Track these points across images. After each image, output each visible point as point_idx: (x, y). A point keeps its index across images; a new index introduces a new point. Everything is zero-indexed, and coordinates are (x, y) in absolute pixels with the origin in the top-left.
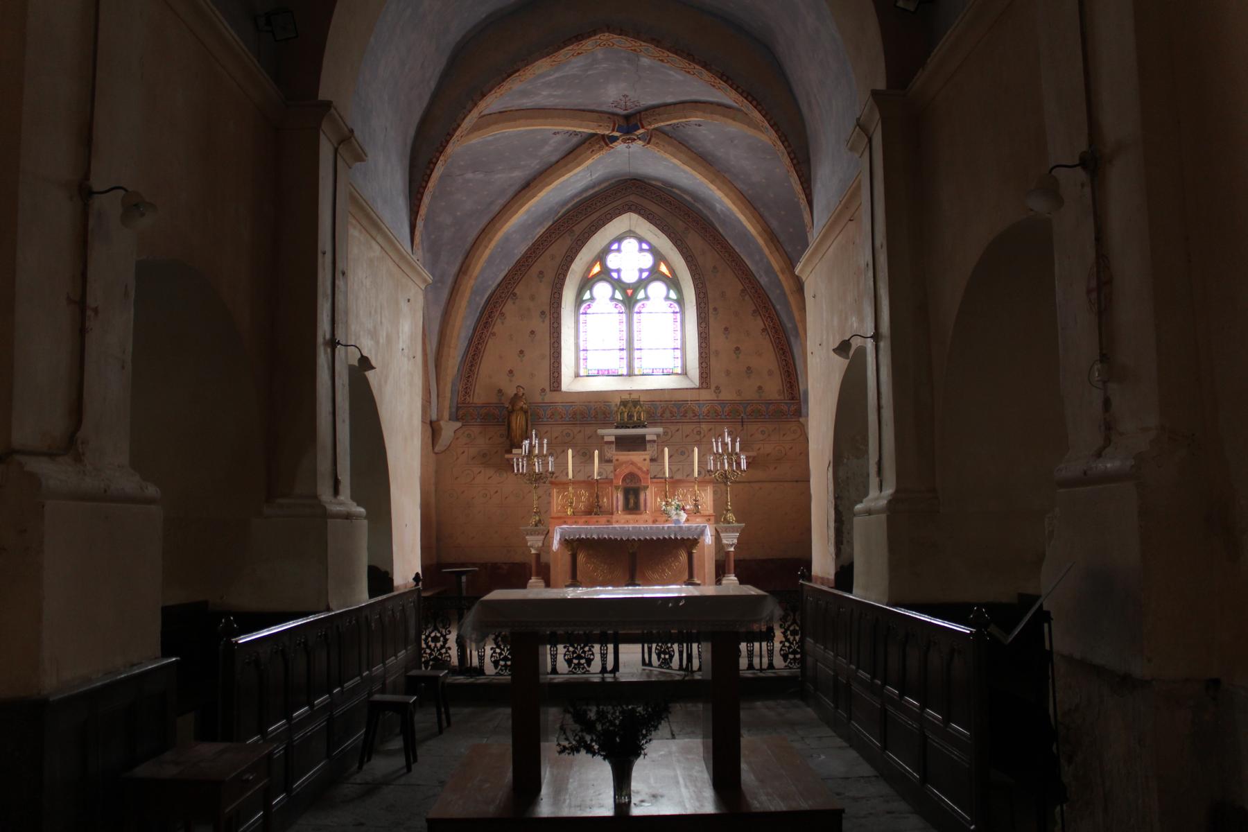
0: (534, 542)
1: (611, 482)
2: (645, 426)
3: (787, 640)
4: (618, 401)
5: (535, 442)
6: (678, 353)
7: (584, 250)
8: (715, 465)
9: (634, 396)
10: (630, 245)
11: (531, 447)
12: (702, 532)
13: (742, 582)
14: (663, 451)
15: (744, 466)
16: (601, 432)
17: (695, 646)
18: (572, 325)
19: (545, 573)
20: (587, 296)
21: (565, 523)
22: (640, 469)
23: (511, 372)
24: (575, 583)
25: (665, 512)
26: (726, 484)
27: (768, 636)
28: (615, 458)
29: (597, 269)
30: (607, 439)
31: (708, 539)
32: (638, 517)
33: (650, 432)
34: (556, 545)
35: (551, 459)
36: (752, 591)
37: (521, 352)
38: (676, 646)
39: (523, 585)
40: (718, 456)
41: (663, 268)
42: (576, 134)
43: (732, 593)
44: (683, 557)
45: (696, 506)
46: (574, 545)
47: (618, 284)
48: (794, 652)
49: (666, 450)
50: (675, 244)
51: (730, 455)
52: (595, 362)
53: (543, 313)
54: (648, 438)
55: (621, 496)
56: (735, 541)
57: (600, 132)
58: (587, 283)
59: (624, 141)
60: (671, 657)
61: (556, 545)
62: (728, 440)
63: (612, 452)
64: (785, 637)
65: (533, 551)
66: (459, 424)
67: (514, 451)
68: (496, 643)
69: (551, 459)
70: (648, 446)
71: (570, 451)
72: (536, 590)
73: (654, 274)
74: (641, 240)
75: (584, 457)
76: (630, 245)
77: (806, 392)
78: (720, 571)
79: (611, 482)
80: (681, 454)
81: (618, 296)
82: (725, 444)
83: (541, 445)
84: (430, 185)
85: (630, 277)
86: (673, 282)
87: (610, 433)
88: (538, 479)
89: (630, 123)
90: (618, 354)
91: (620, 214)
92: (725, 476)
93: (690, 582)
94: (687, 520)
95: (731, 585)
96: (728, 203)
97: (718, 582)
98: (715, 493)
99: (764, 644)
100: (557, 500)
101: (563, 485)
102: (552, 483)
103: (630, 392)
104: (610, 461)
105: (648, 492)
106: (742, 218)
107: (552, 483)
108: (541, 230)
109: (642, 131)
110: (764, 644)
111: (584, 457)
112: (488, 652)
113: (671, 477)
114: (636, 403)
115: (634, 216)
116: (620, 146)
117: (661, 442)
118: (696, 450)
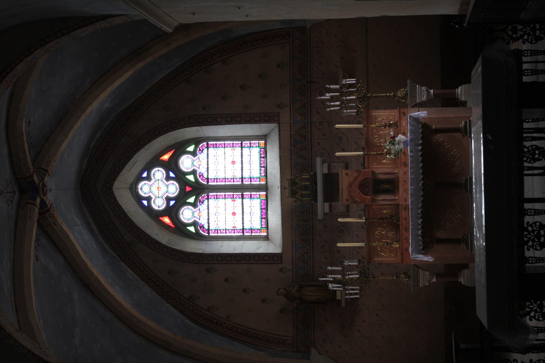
0: (425, 279)
1: (367, 206)
2: (315, 174)
3: (522, 37)
4: (291, 200)
5: (330, 277)
6: (246, 143)
7: (155, 237)
8: (351, 108)
9: (287, 184)
10: (144, 188)
11: (335, 281)
12: (416, 120)
13: (467, 80)
14: (339, 157)
15: (352, 81)
16: (320, 216)
17: (526, 125)
18: (220, 243)
19: (453, 270)
20: (192, 229)
21: (407, 249)
22: (355, 179)
23: (263, 301)
24: (467, 239)
25: (397, 154)
26: (370, 98)
27: (519, 54)
28: (345, 202)
29: (167, 220)
30: (327, 210)
31: (422, 114)
32: (401, 180)
33: (321, 169)
34: (428, 259)
35: (346, 263)
36: (477, 71)
37: (245, 291)
38: (527, 144)
39: (471, 291)
40: (344, 105)
41: (166, 157)
42: (37, 240)
43: (480, 91)
44: (440, 137)
45: (390, 126)
46: (427, 244)
47: (181, 200)
48: (534, 30)
49: (338, 154)
50: (142, 146)
51: (343, 94)
52: (254, 221)
53: (208, 271)
54: (326, 171)
55: (381, 197)
56: (424, 88)
57: (36, 217)
58: (180, 228)
59: (45, 194)
60: (537, 148)
61: (428, 259)
62: (328, 96)
63: (340, 206)
64: (518, 39)
65: (434, 280)
66: (313, 351)
67: (338, 297)
68: (525, 316)
69: (346, 263)
70: (334, 171)
71: (339, 245)
72: (477, 276)
73: (172, 167)
74: (140, 179)
75: (345, 231)
76: (144, 188)
77: (283, 22)
78: (453, 102)
79: (367, 206)
80: (343, 140)
81: (192, 200)
82: (333, 99)
83: (333, 272)
84: (103, 283)
85: (173, 189)
86: (179, 149)
87: (322, 208)
88: (365, 276)
89: (28, 189)
90: (247, 201)
91: (114, 198)
92: (362, 99)
93: (466, 132)
94: (404, 134)
95: (470, 93)
96: (103, 96)
97: (463, 104)
98: (378, 108)
99: (524, 59)
100: (385, 257)
101: (371, 251)
102: (369, 262)
103: (283, 188)
104: (348, 207)
105: (378, 171)
106: (117, 83)
107: (369, 262)
108: (130, 273)
109: (35, 178)
110: (524, 59)
111: (345, 231)
112: (533, 323)
113: (363, 150)
114: (293, 183)
115: (116, 184)
116: (50, 198)
117: (330, 159)
118: (337, 126)
